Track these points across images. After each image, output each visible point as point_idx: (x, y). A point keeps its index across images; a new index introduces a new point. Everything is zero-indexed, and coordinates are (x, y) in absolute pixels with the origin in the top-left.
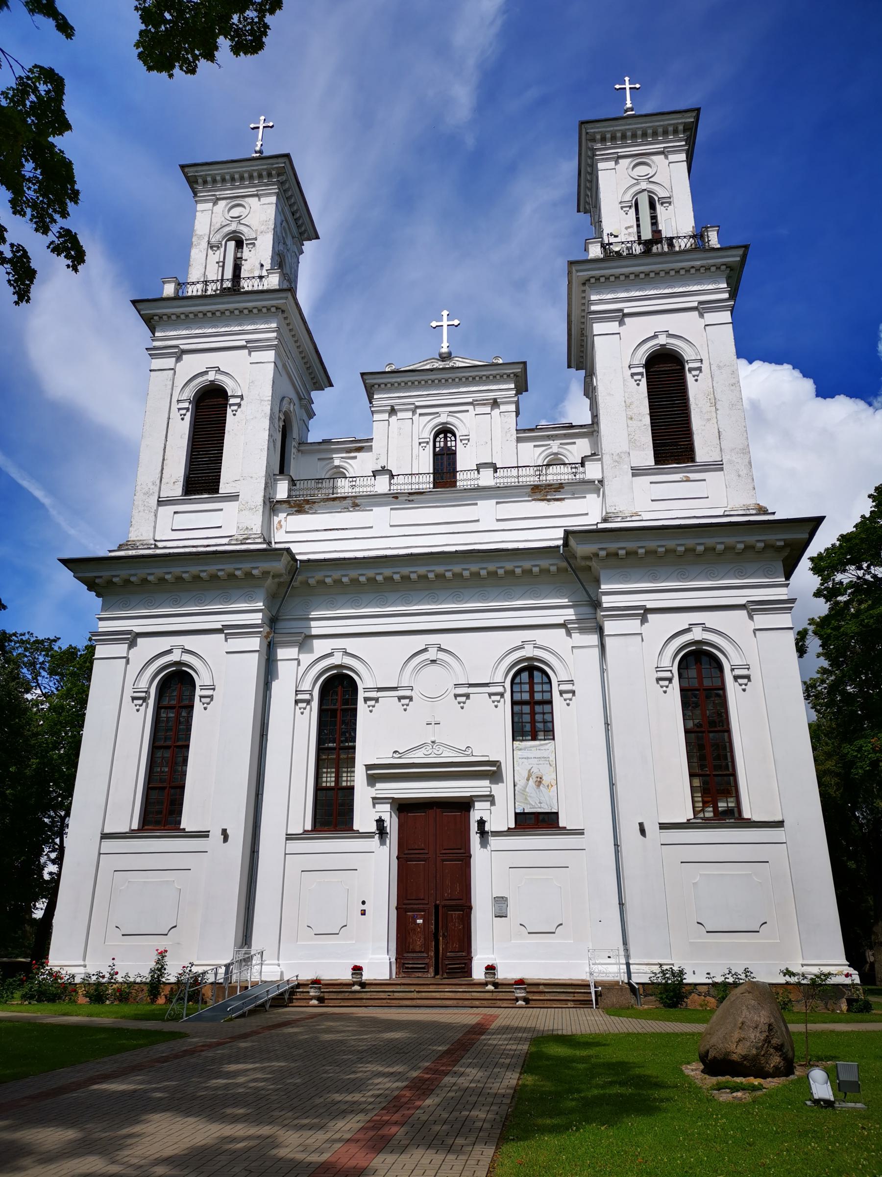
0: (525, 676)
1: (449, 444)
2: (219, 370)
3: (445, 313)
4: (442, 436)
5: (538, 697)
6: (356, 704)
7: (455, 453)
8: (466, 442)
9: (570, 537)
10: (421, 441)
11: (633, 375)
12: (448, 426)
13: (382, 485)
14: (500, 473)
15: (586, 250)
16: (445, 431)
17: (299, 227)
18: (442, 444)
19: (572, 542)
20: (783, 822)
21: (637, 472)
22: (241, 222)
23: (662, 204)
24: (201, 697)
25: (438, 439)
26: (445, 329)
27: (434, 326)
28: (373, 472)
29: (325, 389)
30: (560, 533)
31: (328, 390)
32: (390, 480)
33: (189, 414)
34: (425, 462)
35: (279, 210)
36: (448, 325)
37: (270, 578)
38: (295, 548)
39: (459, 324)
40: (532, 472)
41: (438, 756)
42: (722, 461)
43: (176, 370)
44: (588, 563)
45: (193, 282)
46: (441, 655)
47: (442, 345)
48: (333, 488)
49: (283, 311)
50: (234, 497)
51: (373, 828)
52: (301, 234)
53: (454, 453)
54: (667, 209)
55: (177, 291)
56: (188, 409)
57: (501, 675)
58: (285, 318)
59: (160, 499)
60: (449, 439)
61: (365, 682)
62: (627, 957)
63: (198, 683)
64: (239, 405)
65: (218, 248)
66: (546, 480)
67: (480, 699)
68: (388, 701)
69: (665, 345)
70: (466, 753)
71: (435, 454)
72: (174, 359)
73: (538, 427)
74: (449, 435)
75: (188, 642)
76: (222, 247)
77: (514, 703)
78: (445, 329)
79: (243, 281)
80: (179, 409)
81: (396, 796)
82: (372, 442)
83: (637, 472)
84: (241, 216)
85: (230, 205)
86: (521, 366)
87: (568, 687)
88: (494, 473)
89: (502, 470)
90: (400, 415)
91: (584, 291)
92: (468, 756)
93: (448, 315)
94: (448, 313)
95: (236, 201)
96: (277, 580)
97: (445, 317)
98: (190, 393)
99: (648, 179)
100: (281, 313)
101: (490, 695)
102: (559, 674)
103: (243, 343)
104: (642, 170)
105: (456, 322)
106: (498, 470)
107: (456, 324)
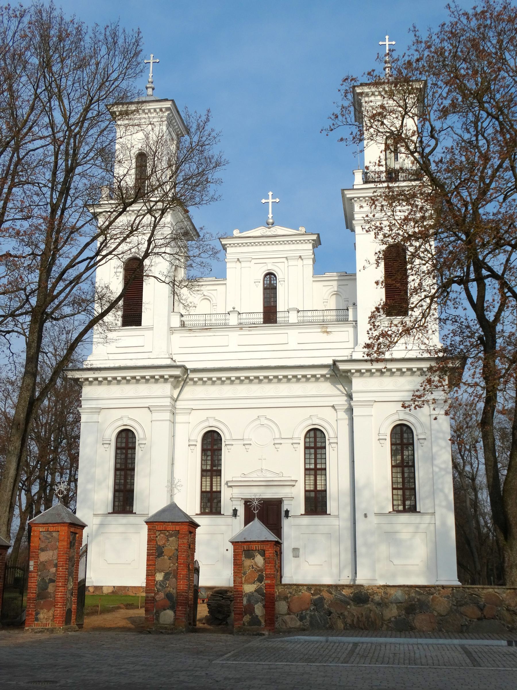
1: (272, 282)
3: (270, 194)
5: (319, 445)
7: (276, 289)
16: (270, 275)
18: (268, 282)
25: (266, 279)
34: (260, 307)
44: (346, 374)
50: (151, 328)
60: (272, 279)
61: (226, 437)
67: (287, 446)
86: (316, 236)
90: (243, 264)
97: (270, 197)
102: (329, 434)
105: (278, 200)
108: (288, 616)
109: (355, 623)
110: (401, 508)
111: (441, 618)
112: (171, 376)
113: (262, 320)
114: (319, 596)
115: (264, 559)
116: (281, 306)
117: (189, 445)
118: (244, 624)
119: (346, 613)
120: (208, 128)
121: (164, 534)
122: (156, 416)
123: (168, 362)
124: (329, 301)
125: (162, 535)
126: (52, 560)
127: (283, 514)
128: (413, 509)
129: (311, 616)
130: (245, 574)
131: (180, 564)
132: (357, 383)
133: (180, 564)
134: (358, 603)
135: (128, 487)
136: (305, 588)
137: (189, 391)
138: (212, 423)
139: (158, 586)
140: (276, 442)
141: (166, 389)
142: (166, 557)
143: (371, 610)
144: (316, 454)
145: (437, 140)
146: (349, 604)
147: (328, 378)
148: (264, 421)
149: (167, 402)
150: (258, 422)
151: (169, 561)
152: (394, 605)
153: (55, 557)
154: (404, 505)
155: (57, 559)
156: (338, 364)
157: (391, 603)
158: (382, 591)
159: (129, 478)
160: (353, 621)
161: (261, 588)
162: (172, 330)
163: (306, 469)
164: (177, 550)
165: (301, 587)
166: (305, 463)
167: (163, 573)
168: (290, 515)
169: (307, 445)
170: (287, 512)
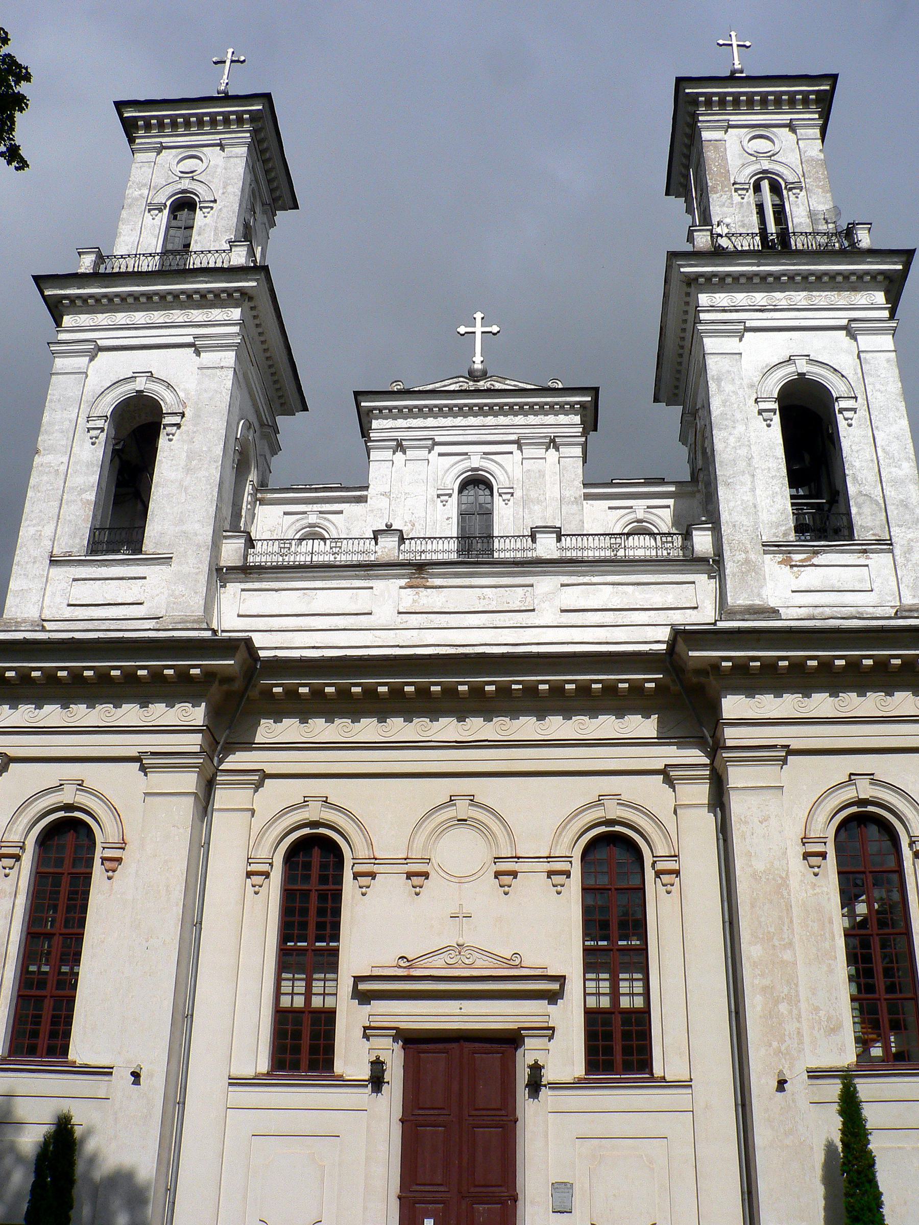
2: (152, 376)
3: (479, 316)
6: (91, 866)
8: (508, 496)
9: (679, 639)
10: (440, 492)
11: (760, 412)
12: (480, 472)
13: (387, 548)
14: (566, 542)
15: (690, 239)
17: (272, 191)
19: (681, 646)
22: (194, 177)
23: (791, 189)
24: (104, 859)
26: (478, 337)
27: (462, 332)
28: (374, 532)
29: (297, 414)
30: (664, 634)
31: (300, 415)
32: (246, 550)
33: (103, 436)
35: (251, 168)
36: (483, 333)
37: (217, 683)
38: (258, 640)
39: (498, 332)
40: (276, 548)
41: (469, 966)
42: (890, 540)
43: (88, 373)
44: (703, 680)
45: (122, 256)
47: (474, 359)
48: (312, 553)
49: (251, 299)
52: (275, 200)
54: (797, 197)
55: (96, 264)
56: (102, 430)
58: (252, 308)
59: (52, 559)
63: (99, 838)
64: (178, 426)
65: (160, 210)
66: (657, 556)
69: (804, 374)
70: (511, 962)
72: (88, 358)
73: (614, 481)
76: (165, 208)
78: (478, 337)
79: (194, 256)
80: (89, 430)
81: (403, 1026)
82: (367, 490)
84: (195, 171)
85: (180, 157)
87: (671, 865)
88: (557, 542)
89: (568, 538)
91: (688, 294)
92: (515, 967)
93: (483, 318)
94: (483, 315)
95: (192, 152)
96: (225, 687)
97: (479, 322)
98: (107, 406)
99: (770, 157)
100: (247, 300)
103: (190, 340)
104: (762, 145)
105: (495, 329)
106: (563, 538)
107: (495, 332)
127: (522, 1076)
128: (229, 1085)
150: (450, 813)
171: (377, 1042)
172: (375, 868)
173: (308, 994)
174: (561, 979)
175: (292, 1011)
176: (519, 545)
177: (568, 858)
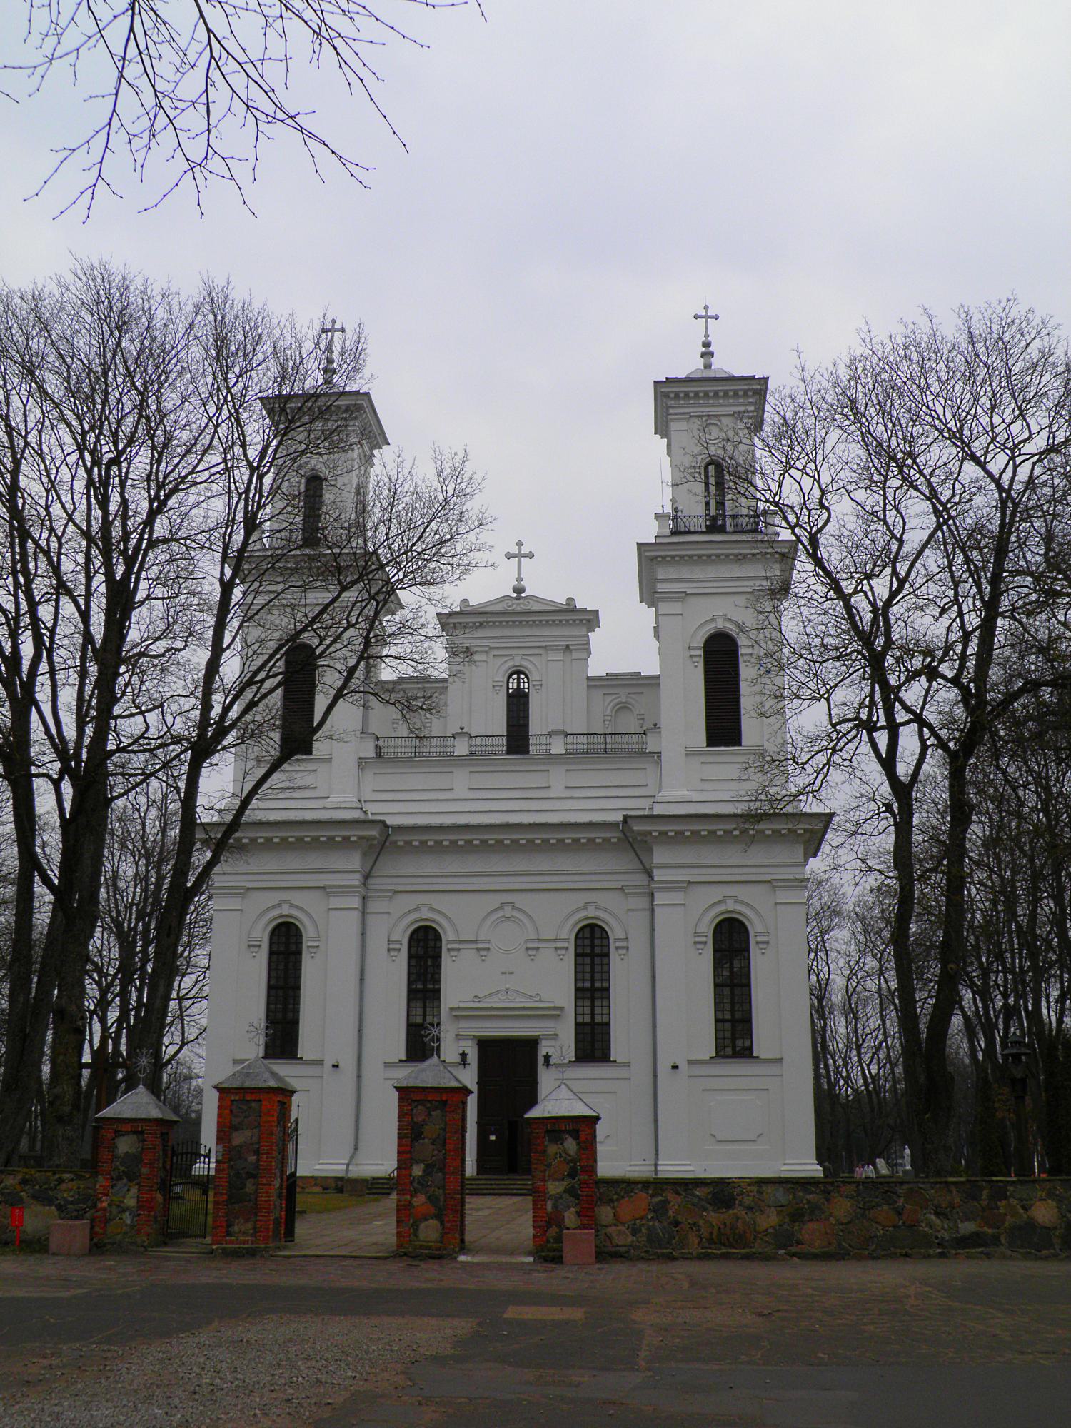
0: (587, 931)
4: (515, 676)
20: (746, 1053)
21: (690, 753)
34: (499, 725)
46: (515, 914)
51: (458, 1059)
53: (526, 696)
57: (568, 934)
61: (448, 936)
62: (657, 1158)
67: (547, 955)
68: (468, 954)
71: (509, 696)
74: (522, 676)
75: (297, 898)
77: (577, 955)
83: (690, 753)
101: (556, 949)
102: (615, 933)
108: (614, 1228)
109: (714, 1236)
110: (729, 1051)
111: (841, 1227)
112: (361, 838)
113: (504, 748)
114: (660, 1198)
115: (578, 1144)
116: (535, 726)
117: (389, 950)
118: (548, 1241)
119: (701, 1222)
120: (469, 467)
121: (424, 1105)
122: (336, 902)
123: (357, 814)
124: (544, 682)
125: (420, 1107)
126: (252, 1144)
127: (541, 1060)
128: (746, 1053)
129: (648, 1228)
130: (549, 1166)
131: (450, 1151)
132: (661, 856)
133: (450, 1151)
134: (719, 1208)
135: (290, 1015)
136: (640, 1186)
137: (389, 865)
138: (425, 914)
139: (415, 1184)
140: (529, 945)
141: (354, 860)
142: (426, 1140)
143: (738, 1218)
144: (593, 965)
145: (828, 509)
146: (705, 1209)
147: (614, 844)
148: (508, 911)
149: (356, 879)
150: (501, 914)
151: (431, 1147)
152: (773, 1209)
153: (255, 1139)
154: (734, 1047)
155: (259, 1143)
156: (628, 820)
157: (769, 1206)
158: (755, 1189)
159: (292, 1002)
160: (711, 1233)
161: (573, 1187)
162: (362, 762)
163: (577, 990)
164: (444, 1130)
165: (633, 1186)
166: (576, 980)
167: (423, 1166)
168: (551, 1062)
169: (580, 951)
170: (547, 1057)
171: (463, 1043)
172: (461, 946)
173: (593, 1014)
174: (561, 1009)
175: (584, 1024)
176: (490, 742)
177: (567, 940)
